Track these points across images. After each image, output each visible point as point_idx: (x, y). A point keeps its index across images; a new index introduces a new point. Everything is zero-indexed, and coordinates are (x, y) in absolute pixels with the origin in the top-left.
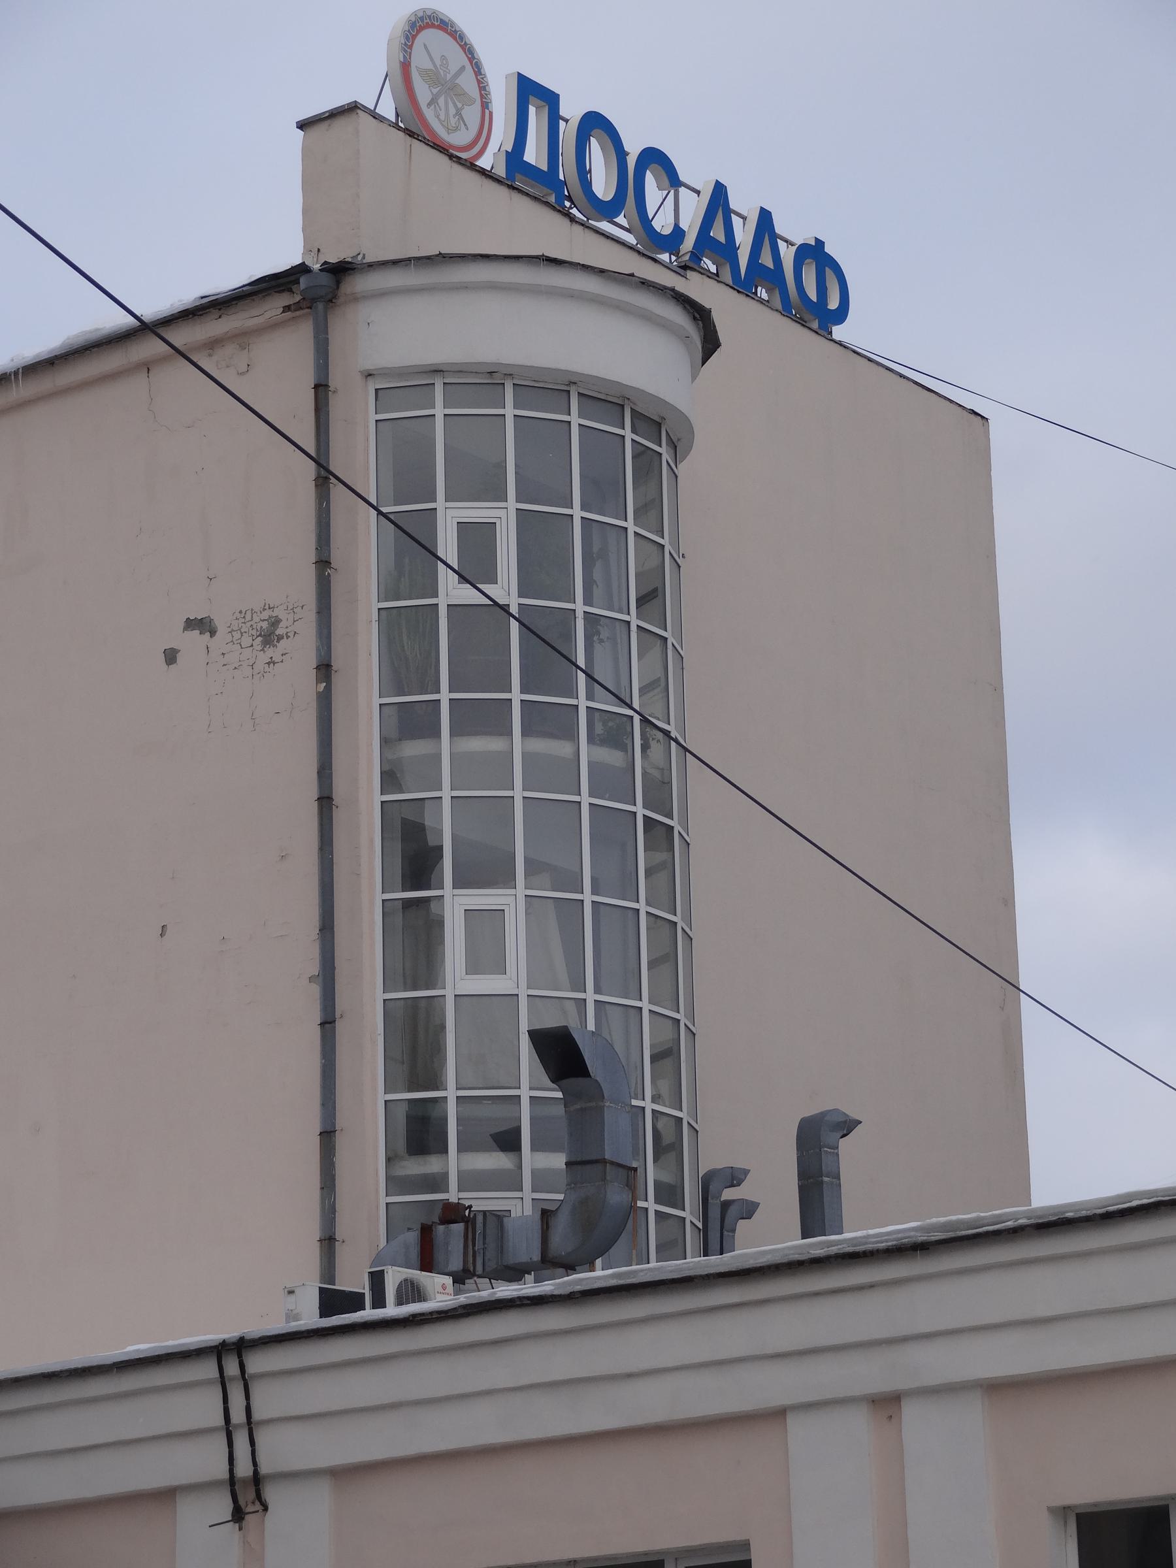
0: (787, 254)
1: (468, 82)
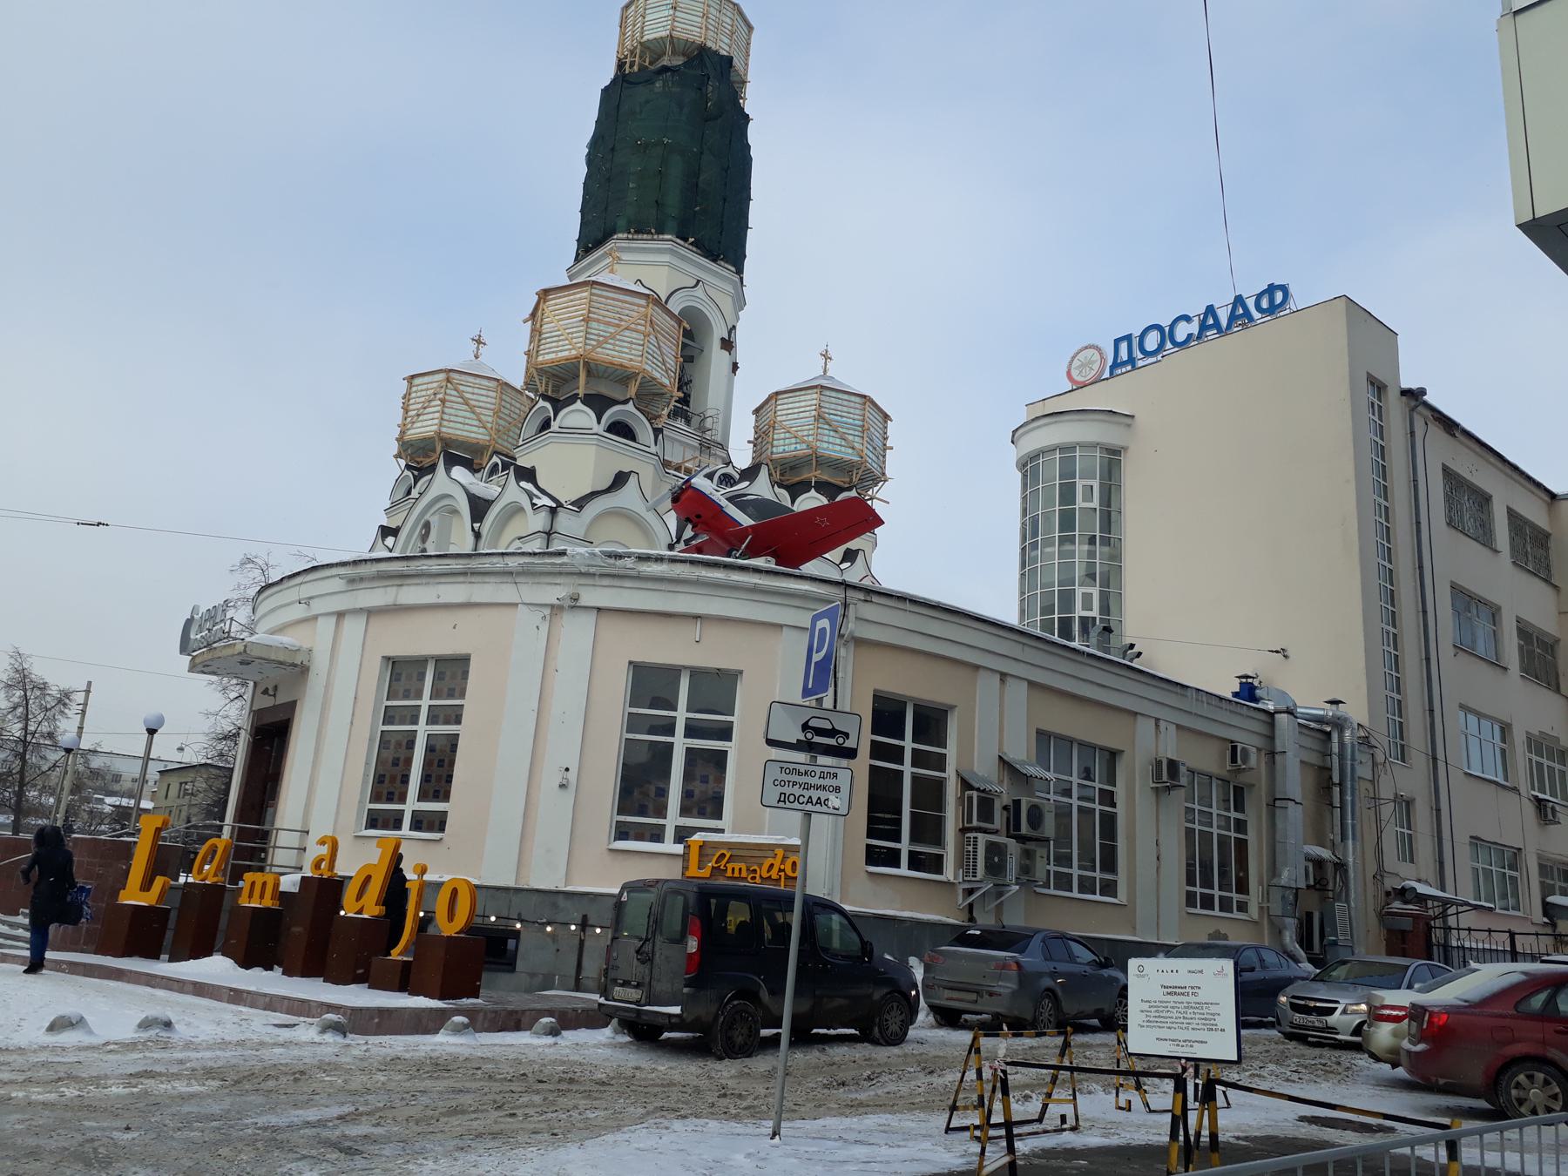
1: (1076, 363)
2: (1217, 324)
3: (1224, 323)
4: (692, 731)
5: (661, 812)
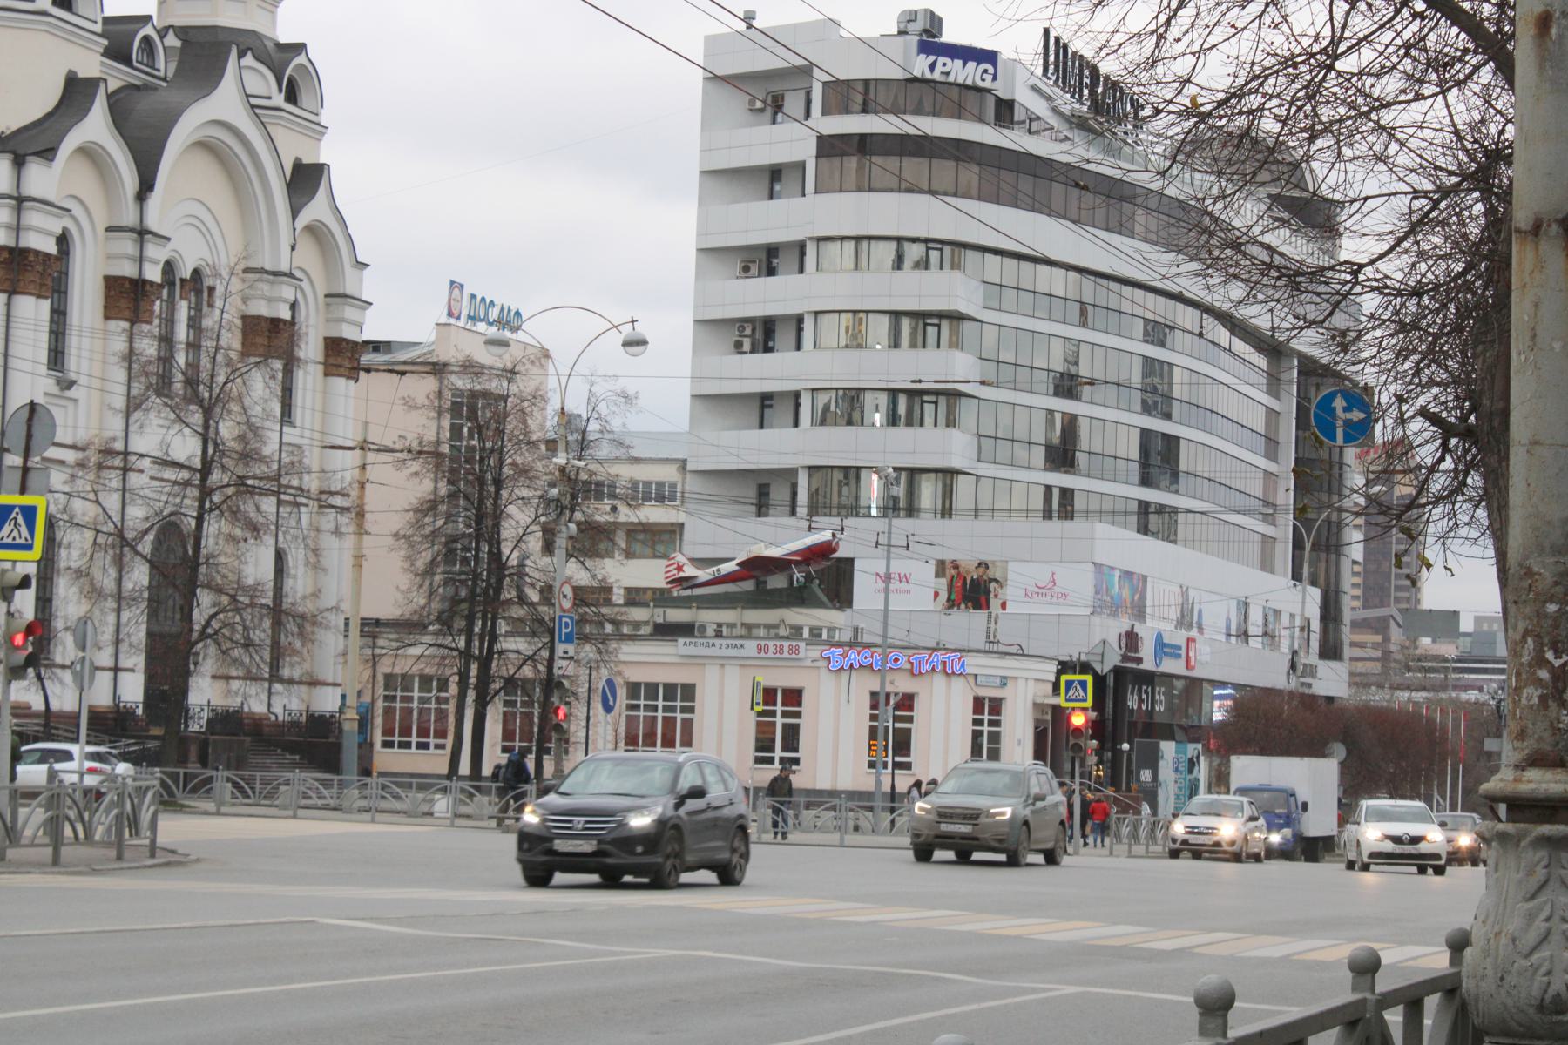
4: (785, 714)
5: (772, 750)
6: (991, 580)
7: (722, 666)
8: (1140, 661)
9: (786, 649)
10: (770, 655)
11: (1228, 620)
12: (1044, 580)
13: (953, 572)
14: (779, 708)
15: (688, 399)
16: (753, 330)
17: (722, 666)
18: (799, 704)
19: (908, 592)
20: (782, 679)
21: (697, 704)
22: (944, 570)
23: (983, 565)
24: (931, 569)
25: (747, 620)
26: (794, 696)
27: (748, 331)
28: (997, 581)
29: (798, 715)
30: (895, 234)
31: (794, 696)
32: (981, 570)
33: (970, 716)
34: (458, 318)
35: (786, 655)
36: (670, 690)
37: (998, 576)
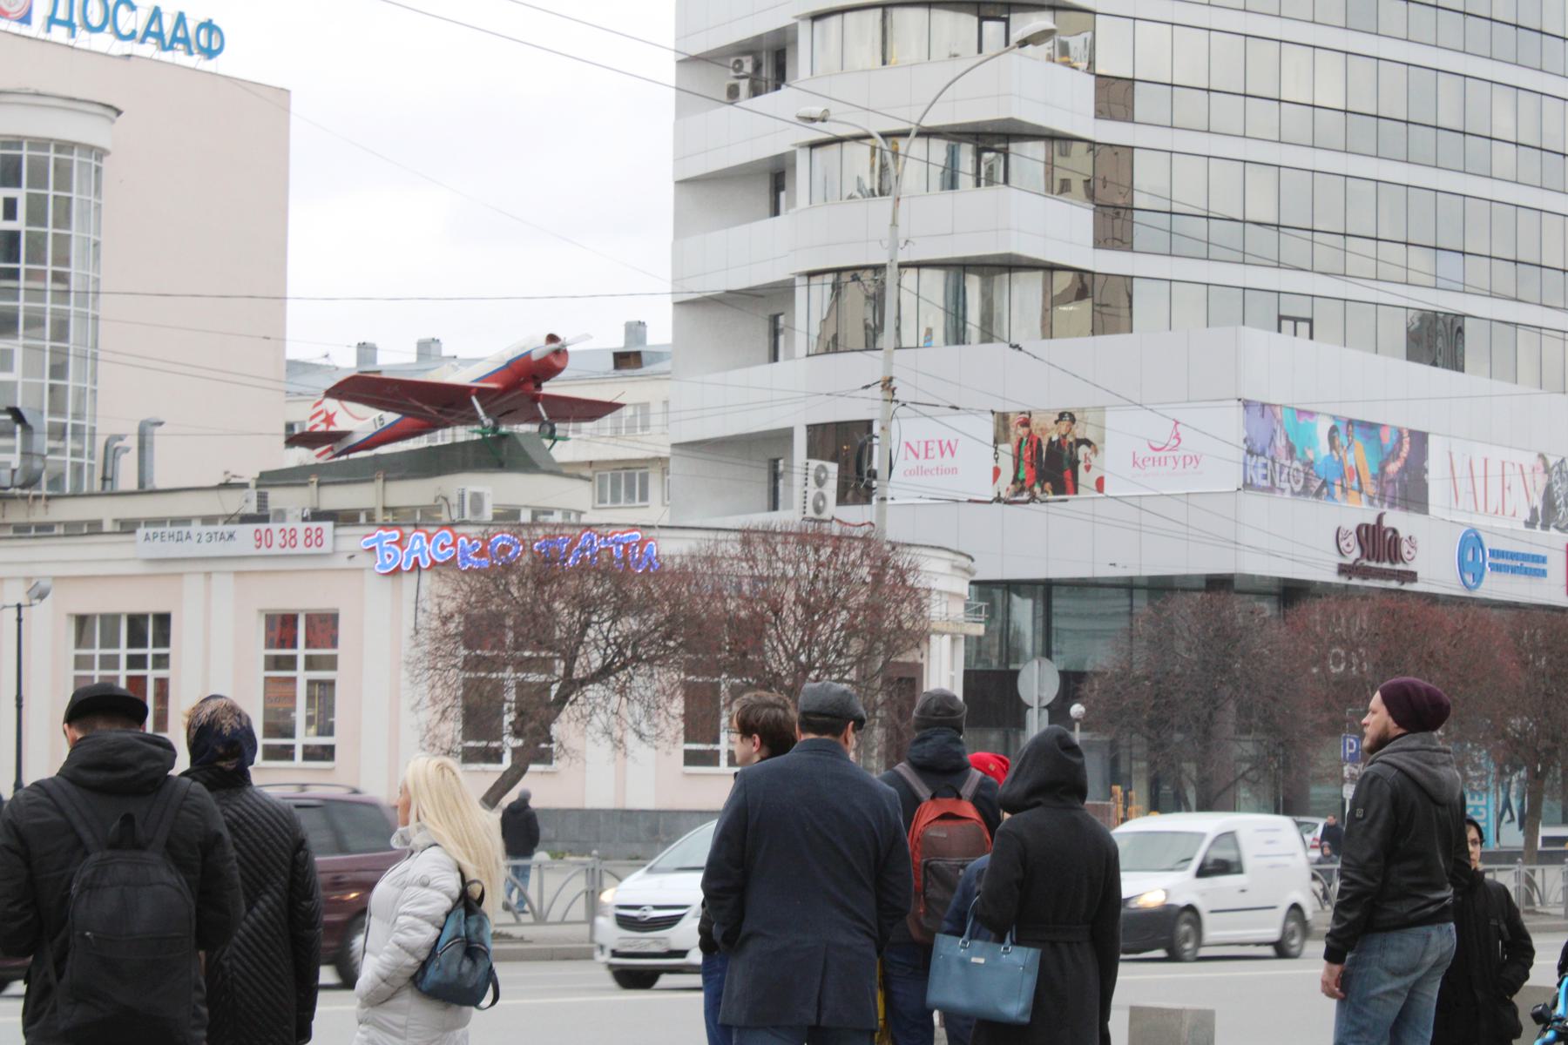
0: (191, 26)
2: (159, 36)
3: (168, 38)
6: (1080, 442)
7: (208, 574)
8: (1412, 576)
9: (301, 536)
10: (275, 550)
11: (588, 337)
12: (1163, 434)
13: (1022, 431)
14: (301, 652)
15: (670, 189)
16: (757, 67)
17: (208, 574)
18: (334, 643)
19: (954, 471)
20: (302, 597)
21: (342, 652)
22: (1006, 428)
23: (1066, 417)
24: (987, 429)
25: (392, 502)
26: (325, 627)
27: (748, 68)
28: (1088, 443)
29: (331, 662)
30: (1350, 33)
31: (325, 627)
32: (1063, 426)
33: (259, 650)
34: (26, 19)
35: (301, 548)
36: (136, 623)
37: (1090, 436)
